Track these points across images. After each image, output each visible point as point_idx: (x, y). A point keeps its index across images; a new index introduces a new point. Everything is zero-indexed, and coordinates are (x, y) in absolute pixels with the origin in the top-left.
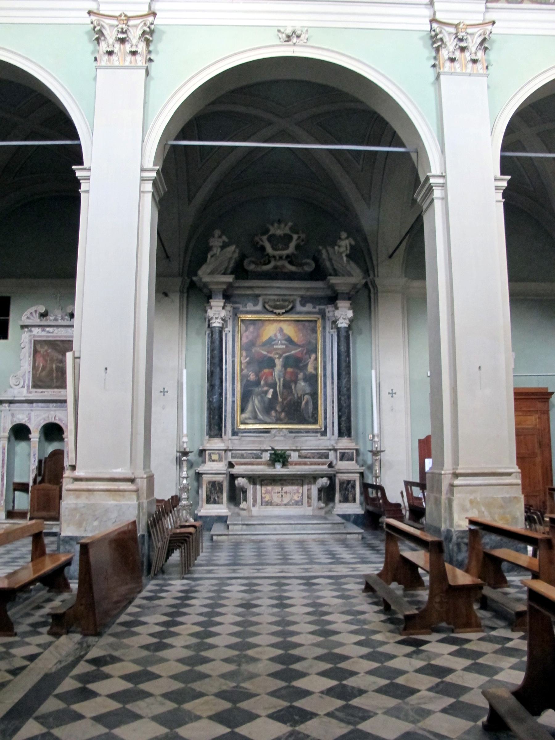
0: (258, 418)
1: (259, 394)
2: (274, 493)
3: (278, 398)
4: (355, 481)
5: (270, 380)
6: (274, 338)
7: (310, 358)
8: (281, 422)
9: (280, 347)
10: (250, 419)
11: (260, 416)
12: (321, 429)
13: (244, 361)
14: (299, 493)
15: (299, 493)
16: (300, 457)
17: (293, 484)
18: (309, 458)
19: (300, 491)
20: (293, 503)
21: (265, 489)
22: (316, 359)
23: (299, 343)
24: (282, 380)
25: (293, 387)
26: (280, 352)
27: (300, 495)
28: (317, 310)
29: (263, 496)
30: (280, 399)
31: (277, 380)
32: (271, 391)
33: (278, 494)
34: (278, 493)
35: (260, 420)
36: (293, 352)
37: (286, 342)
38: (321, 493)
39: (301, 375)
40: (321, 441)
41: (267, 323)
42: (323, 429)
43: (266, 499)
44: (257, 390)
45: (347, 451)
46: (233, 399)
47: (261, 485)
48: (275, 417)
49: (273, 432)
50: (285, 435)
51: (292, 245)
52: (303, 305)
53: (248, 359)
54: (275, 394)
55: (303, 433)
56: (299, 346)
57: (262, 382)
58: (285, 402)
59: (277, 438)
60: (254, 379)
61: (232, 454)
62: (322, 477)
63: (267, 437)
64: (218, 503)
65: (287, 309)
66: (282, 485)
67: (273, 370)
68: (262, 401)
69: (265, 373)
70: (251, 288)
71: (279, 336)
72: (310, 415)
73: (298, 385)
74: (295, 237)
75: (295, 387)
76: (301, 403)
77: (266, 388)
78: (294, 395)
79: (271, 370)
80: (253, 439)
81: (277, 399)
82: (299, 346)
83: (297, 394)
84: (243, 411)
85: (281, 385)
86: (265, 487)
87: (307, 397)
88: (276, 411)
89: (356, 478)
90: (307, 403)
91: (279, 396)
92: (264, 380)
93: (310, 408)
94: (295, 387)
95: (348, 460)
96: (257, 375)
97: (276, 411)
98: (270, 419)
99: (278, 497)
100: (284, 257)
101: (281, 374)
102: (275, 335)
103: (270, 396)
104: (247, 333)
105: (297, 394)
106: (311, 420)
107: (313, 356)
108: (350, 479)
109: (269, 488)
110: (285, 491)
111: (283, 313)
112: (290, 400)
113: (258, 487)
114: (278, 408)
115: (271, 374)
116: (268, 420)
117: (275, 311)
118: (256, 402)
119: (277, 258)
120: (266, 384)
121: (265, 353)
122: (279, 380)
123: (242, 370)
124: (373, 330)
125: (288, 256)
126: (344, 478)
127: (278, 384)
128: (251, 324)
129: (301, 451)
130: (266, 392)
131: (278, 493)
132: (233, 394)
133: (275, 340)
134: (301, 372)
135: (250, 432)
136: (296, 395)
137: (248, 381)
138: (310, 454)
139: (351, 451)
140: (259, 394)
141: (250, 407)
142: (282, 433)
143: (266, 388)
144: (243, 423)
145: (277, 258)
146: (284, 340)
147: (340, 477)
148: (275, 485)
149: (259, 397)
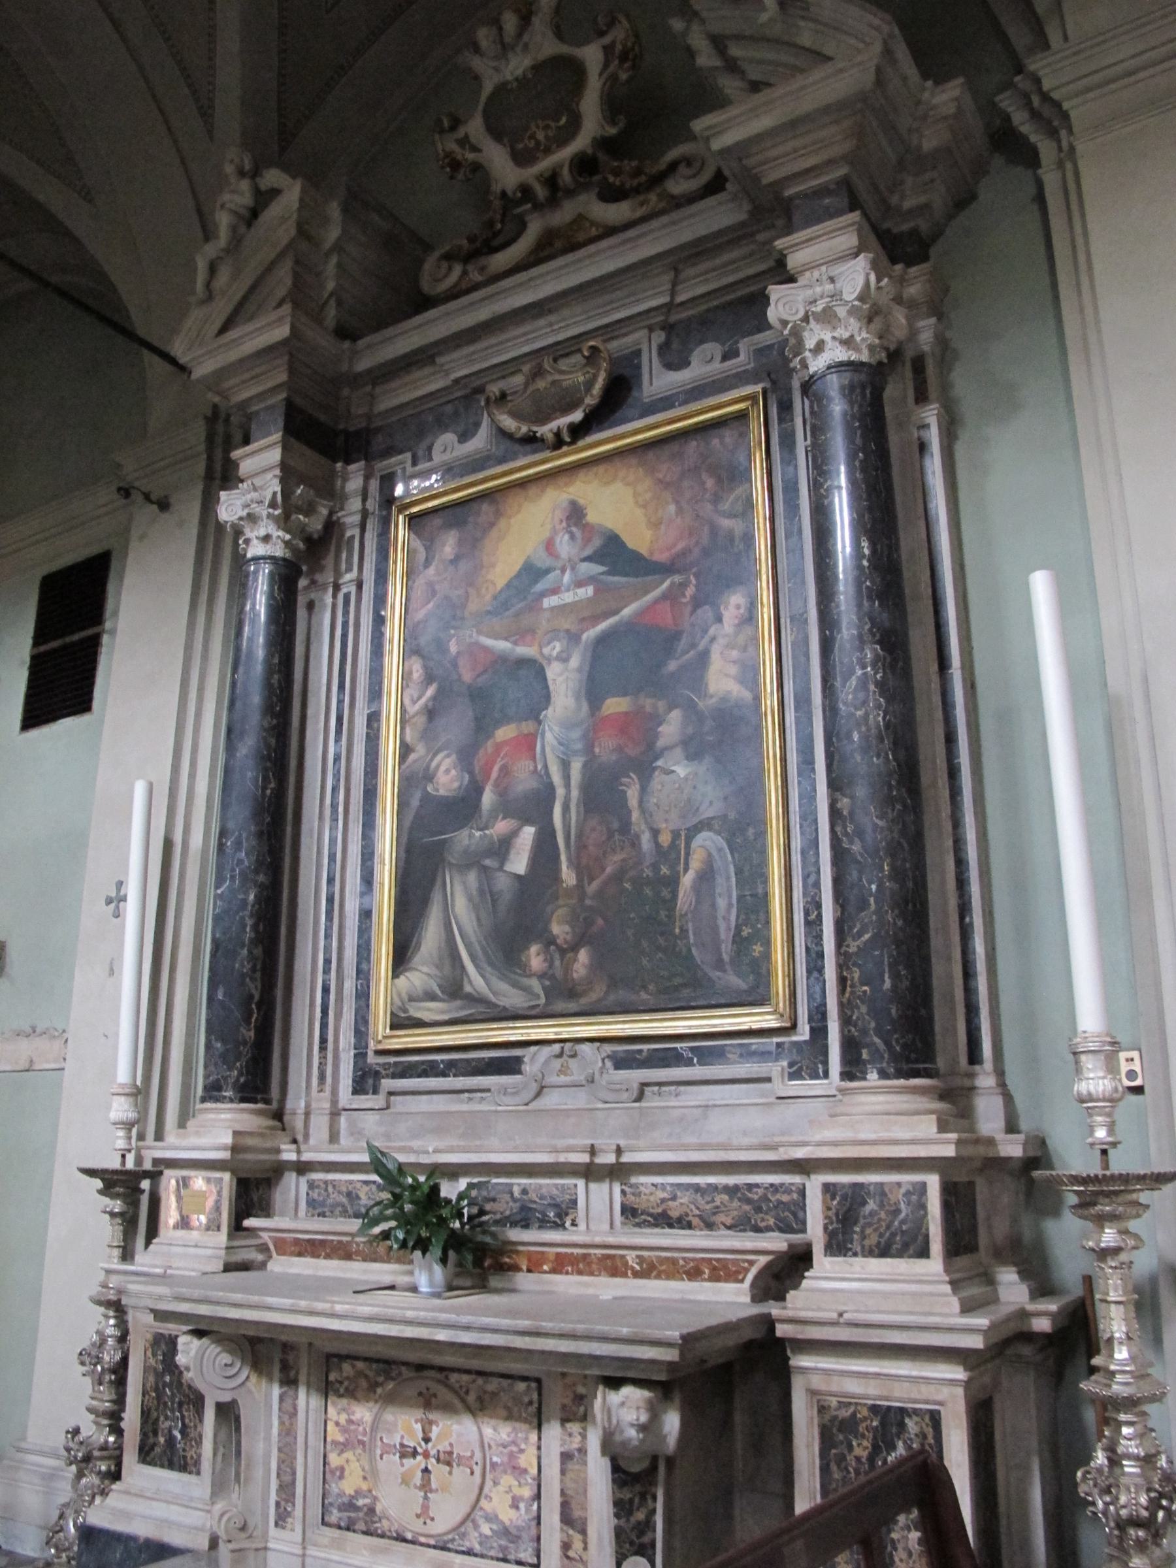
0: (468, 989)
1: (471, 861)
2: (387, 1449)
3: (558, 870)
4: (935, 1419)
5: (524, 781)
6: (548, 562)
7: (719, 619)
8: (572, 1006)
9: (568, 597)
10: (431, 997)
11: (476, 981)
12: (794, 1027)
13: (412, 709)
14: (519, 1472)
15: (519, 1472)
16: (629, 1212)
17: (480, 1406)
18: (682, 1223)
19: (527, 1460)
20: (483, 1540)
21: (343, 1418)
22: (750, 618)
23: (662, 557)
24: (576, 766)
25: (632, 795)
26: (567, 624)
27: (527, 1492)
28: (743, 360)
29: (334, 1460)
30: (568, 876)
31: (557, 779)
32: (528, 833)
33: (409, 1462)
34: (408, 1453)
35: (475, 999)
36: (627, 612)
37: (596, 569)
38: (647, 1496)
39: (671, 728)
40: (791, 1111)
41: (513, 501)
42: (804, 1033)
43: (348, 1486)
44: (467, 838)
45: (330, 1237)
46: (366, 899)
47: (327, 1389)
48: (542, 976)
49: (533, 1061)
50: (591, 1080)
51: (590, 105)
52: (675, 360)
53: (430, 692)
54: (545, 849)
55: (689, 1063)
56: (666, 569)
57: (488, 798)
58: (592, 888)
59: (551, 1100)
60: (456, 785)
61: (312, 1185)
62: (614, 1383)
63: (504, 1091)
64: (183, 1468)
65: (591, 401)
66: (428, 1402)
67: (540, 723)
68: (486, 896)
69: (499, 747)
70: (424, 357)
71: (565, 547)
72: (727, 950)
73: (658, 779)
74: (591, 55)
75: (643, 790)
76: (673, 882)
77: (502, 827)
78: (635, 843)
79: (528, 727)
80: (440, 1104)
81: (556, 877)
82: (666, 569)
83: (655, 833)
84: (401, 958)
85: (575, 793)
86: (344, 1402)
87: (706, 842)
88: (550, 942)
89: (944, 1393)
90: (707, 876)
91: (563, 858)
92: (497, 785)
93: (721, 903)
94: (643, 790)
95: (884, 1251)
96: (466, 757)
97: (550, 942)
98: (515, 985)
99: (405, 1481)
100: (566, 176)
101: (576, 734)
102: (549, 546)
103: (519, 864)
104: (431, 570)
105: (655, 833)
106: (735, 981)
107: (734, 604)
108: (899, 1396)
109: (363, 1413)
110: (443, 1446)
111: (578, 431)
112: (618, 877)
113: (306, 1400)
114: (559, 929)
115: (528, 744)
116: (512, 998)
117: (545, 430)
118: (461, 906)
119: (541, 192)
120: (506, 808)
121: (502, 645)
122: (565, 765)
123: (405, 750)
124: (1073, 358)
125: (585, 165)
126: (853, 1387)
127: (560, 792)
128: (449, 526)
129: (634, 1180)
130: (502, 847)
131: (408, 1453)
132: (368, 880)
133: (548, 571)
134: (670, 709)
135: (430, 1070)
136: (646, 840)
137: (426, 798)
138: (684, 1198)
139: (908, 1178)
140: (471, 861)
141: (431, 937)
142: (577, 1074)
143: (502, 827)
144: (398, 1023)
145: (541, 192)
146: (588, 559)
147: (817, 1382)
148: (390, 1399)
149: (472, 877)
